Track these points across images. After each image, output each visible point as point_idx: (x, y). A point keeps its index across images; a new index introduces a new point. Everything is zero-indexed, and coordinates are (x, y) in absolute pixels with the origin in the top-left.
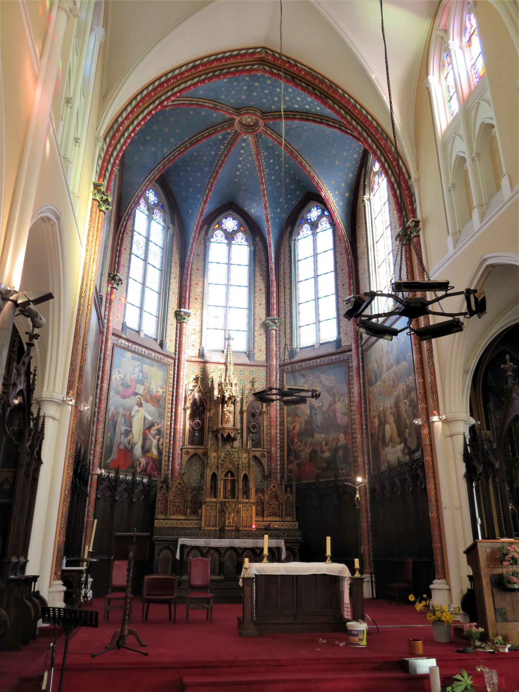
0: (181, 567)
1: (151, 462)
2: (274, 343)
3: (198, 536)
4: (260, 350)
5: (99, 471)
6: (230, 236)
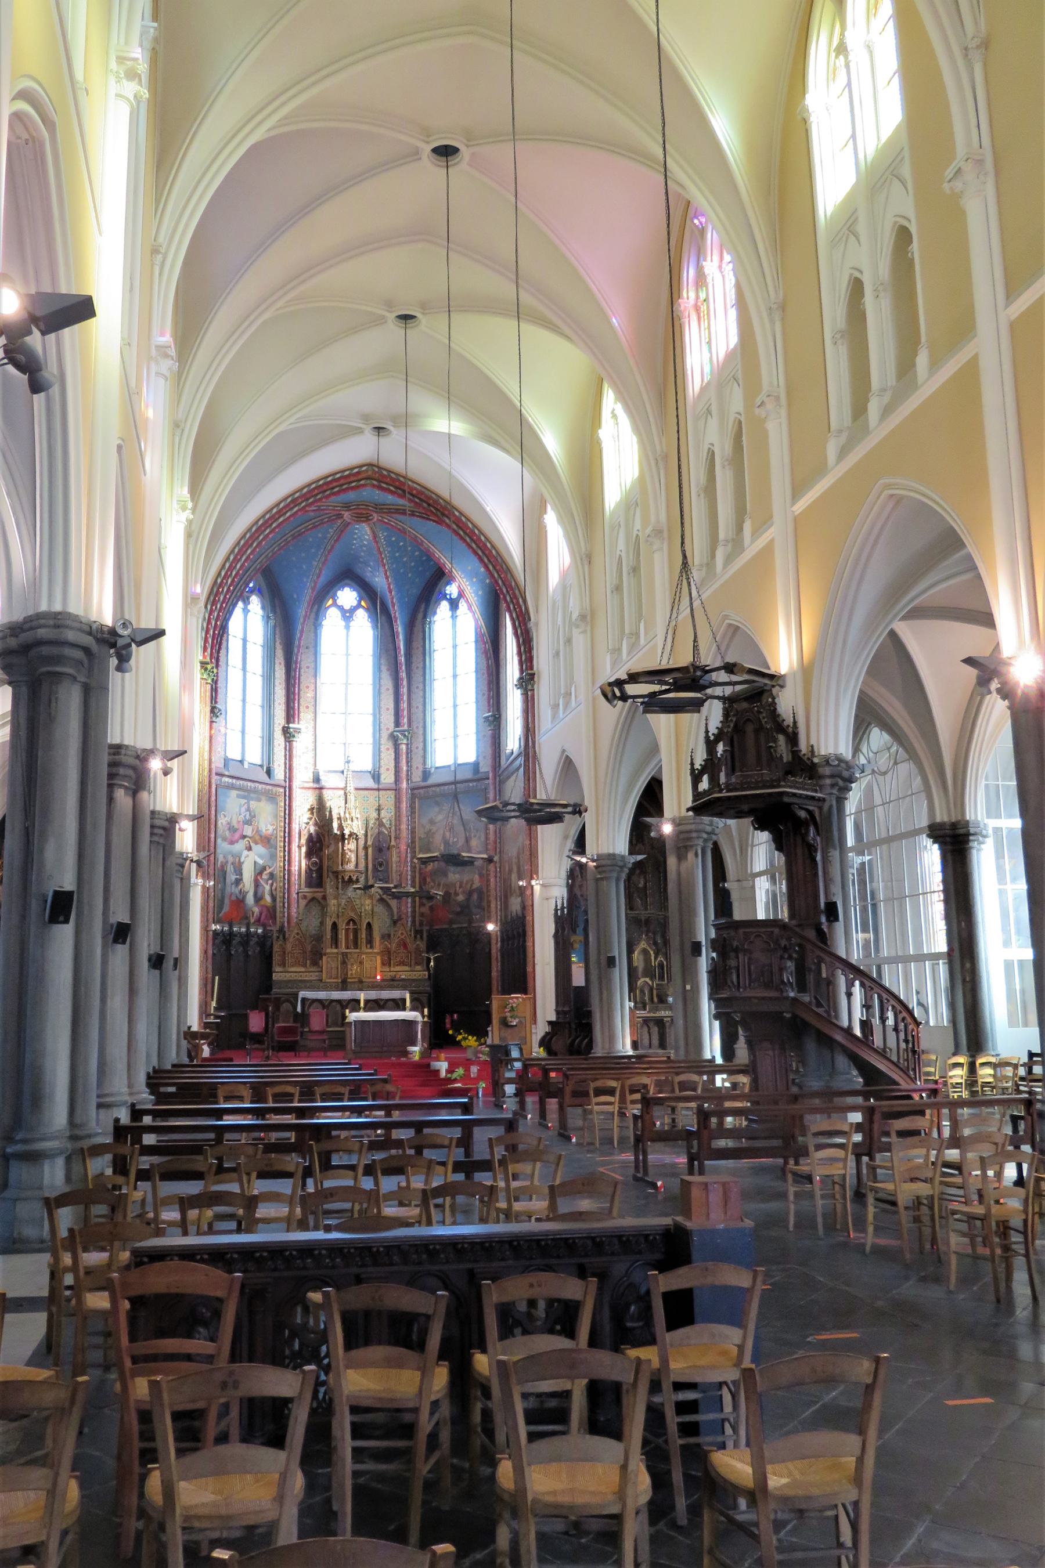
0: (302, 1019)
1: (265, 910)
2: (404, 761)
3: (318, 989)
4: (388, 769)
5: (214, 927)
6: (348, 615)
